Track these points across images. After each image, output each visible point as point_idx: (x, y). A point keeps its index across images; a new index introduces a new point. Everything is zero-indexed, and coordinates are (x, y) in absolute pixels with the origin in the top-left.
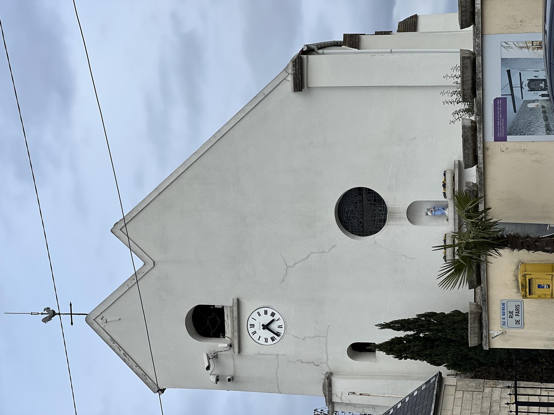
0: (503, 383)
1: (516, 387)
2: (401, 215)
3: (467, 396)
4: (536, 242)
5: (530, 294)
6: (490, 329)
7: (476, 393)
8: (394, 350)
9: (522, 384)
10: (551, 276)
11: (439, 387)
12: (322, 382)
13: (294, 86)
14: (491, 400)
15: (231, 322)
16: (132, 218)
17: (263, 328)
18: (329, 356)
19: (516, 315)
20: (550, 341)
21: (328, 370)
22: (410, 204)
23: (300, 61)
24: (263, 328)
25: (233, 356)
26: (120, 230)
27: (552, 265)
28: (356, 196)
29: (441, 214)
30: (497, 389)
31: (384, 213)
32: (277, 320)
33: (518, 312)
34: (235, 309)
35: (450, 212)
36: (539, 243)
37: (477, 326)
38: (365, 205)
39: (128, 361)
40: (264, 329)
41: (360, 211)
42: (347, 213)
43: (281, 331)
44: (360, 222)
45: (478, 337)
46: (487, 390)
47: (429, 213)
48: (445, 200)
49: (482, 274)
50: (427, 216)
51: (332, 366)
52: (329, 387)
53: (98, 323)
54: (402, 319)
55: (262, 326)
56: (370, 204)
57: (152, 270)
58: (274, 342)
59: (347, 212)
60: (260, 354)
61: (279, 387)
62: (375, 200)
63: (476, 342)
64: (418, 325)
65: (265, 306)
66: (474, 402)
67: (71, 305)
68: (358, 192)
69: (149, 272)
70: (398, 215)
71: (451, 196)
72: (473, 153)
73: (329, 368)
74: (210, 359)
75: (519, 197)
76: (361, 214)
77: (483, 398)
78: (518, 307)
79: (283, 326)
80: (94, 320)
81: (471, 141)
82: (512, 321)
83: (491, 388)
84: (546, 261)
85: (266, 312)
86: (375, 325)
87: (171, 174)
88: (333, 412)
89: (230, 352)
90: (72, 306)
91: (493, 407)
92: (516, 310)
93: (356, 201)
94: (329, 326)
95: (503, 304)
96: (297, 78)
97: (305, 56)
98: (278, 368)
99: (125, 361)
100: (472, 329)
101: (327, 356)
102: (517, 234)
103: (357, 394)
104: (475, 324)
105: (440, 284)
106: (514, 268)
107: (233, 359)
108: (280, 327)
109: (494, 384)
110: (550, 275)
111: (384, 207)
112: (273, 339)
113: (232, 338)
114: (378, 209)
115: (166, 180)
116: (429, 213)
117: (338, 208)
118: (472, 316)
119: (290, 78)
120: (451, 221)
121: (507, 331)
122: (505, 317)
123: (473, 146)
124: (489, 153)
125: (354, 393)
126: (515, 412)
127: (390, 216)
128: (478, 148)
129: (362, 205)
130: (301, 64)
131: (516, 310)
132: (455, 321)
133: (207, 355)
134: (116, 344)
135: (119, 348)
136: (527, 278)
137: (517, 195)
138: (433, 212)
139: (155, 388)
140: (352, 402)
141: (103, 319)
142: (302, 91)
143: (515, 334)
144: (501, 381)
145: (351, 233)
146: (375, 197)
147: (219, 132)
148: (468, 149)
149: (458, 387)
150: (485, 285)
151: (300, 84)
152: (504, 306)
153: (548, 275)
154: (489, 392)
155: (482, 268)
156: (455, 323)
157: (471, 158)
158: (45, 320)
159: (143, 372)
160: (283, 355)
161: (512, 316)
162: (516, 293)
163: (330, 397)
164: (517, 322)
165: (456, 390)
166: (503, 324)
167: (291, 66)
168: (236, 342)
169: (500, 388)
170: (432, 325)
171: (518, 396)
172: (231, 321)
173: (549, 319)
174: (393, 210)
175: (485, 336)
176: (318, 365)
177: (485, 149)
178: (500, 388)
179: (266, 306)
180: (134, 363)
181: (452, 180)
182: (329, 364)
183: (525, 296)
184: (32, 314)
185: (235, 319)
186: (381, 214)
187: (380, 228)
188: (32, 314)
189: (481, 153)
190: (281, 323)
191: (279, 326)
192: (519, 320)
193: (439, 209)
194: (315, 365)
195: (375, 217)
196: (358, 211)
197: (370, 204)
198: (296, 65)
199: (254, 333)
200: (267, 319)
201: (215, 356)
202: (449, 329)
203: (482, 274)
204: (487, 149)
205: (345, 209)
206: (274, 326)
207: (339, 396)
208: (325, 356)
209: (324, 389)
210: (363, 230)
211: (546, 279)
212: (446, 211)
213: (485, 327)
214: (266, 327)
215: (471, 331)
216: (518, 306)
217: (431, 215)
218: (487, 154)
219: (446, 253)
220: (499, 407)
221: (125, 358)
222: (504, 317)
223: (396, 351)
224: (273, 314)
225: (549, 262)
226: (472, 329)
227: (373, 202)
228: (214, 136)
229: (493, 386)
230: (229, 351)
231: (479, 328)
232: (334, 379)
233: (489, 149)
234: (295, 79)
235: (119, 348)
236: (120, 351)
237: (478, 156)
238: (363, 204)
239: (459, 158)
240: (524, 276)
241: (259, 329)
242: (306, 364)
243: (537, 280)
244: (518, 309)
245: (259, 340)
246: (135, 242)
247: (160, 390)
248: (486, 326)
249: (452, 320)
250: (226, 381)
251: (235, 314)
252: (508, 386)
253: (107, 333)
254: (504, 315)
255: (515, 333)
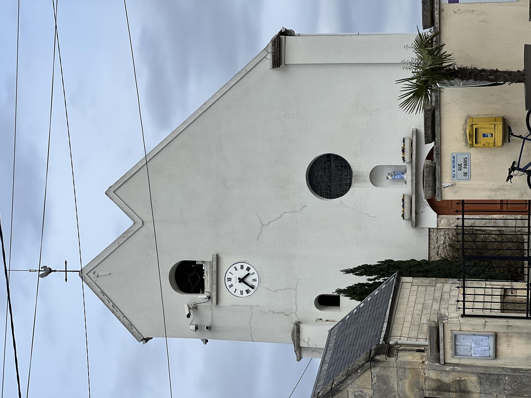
0: (452, 280)
1: (464, 287)
2: (364, 178)
3: (422, 289)
4: (482, 72)
5: (476, 143)
6: (442, 182)
7: (429, 287)
8: (357, 293)
9: (468, 283)
10: (494, 125)
11: (397, 282)
12: (291, 330)
13: (273, 63)
14: (442, 291)
15: (210, 278)
16: (125, 182)
17: (239, 281)
18: (298, 307)
19: (464, 168)
20: (493, 192)
21: (297, 320)
22: (374, 168)
23: (278, 41)
24: (239, 281)
25: (211, 307)
26: (114, 192)
27: (495, 119)
28: (325, 162)
29: (400, 178)
30: (447, 284)
31: (349, 177)
32: (252, 274)
33: (466, 164)
34: (215, 263)
35: (408, 176)
36: (484, 73)
37: (431, 179)
38: (333, 171)
39: (116, 312)
40: (240, 283)
41: (329, 176)
42: (317, 178)
43: (255, 284)
44: (329, 186)
45: (432, 190)
46: (438, 285)
47: (390, 177)
48: (404, 164)
49: (436, 128)
50: (387, 180)
51: (300, 316)
52: (297, 332)
53: (90, 278)
54: (364, 265)
55: (238, 279)
56: (337, 169)
57: (141, 229)
58: (249, 294)
59: (316, 177)
60: (236, 305)
61: (252, 336)
62: (342, 166)
63: (430, 195)
64: (379, 269)
65: (241, 262)
66: (427, 292)
67: (66, 263)
68: (327, 159)
69: (138, 231)
70: (362, 178)
71: (409, 160)
72: (431, 15)
73: (298, 317)
74: (190, 308)
75: (469, 55)
76: (329, 178)
77: (435, 290)
78: (466, 159)
79: (257, 280)
80: (87, 274)
81: (429, 4)
82: (460, 174)
83: (442, 284)
84: (490, 115)
85: (242, 267)
86: (340, 271)
87: (161, 142)
88: (301, 358)
89: (208, 304)
90: (67, 264)
91: (444, 296)
92: (464, 163)
93: (325, 167)
94: (299, 279)
95: (454, 157)
96: (276, 56)
97: (283, 37)
98: (251, 318)
99: (113, 312)
100: (427, 182)
101: (296, 306)
102: (466, 68)
103: (323, 320)
104: (429, 177)
105: (400, 104)
106: (463, 122)
107: (211, 310)
108: (254, 280)
109: (445, 281)
110: (493, 124)
111: (349, 172)
112: (248, 291)
113: (211, 292)
114: (344, 174)
115: (157, 147)
116: (390, 177)
117: (309, 173)
118: (428, 169)
119: (270, 56)
120: (409, 184)
121: (457, 183)
122: (455, 169)
123: (431, 9)
124: (443, 14)
125: (321, 319)
126: (462, 308)
127: (355, 179)
128: (435, 9)
129: (331, 171)
130: (279, 43)
131: (464, 163)
132: (411, 265)
133: (188, 305)
134: (106, 297)
135: (108, 300)
136: (473, 127)
137: (466, 53)
138: (393, 176)
139: (140, 337)
140: (318, 347)
141: (95, 274)
142: (280, 67)
143: (463, 186)
144: (451, 279)
145: (320, 196)
146: (342, 163)
147: (205, 104)
148: (426, 11)
149: (413, 283)
150: (438, 139)
151: (278, 60)
152: (454, 159)
153: (492, 124)
154: (441, 286)
155: (436, 122)
156: (411, 267)
157: (429, 19)
158: (42, 276)
159: (130, 322)
160: (257, 306)
161: (461, 168)
162: (465, 146)
163: (298, 342)
164: (465, 174)
165: (412, 285)
166: (453, 176)
167: (271, 45)
168: (214, 294)
169: (450, 283)
170: (391, 270)
171: (465, 288)
172: (210, 276)
173: (492, 170)
174: (358, 174)
175: (438, 187)
176: (288, 315)
177: (440, 11)
178: (450, 283)
179: (242, 261)
180: (122, 314)
181: (410, 145)
182: (298, 314)
183: (472, 146)
184: (30, 271)
185: (214, 273)
186: (347, 178)
187: (346, 191)
188: (30, 271)
189: (438, 14)
190: (255, 276)
191: (253, 280)
192: (467, 172)
193: (399, 173)
194: (285, 315)
195: (341, 181)
196: (327, 176)
197: (337, 169)
198: (275, 44)
199: (231, 286)
200: (242, 273)
201: (195, 308)
202: (406, 272)
203: (436, 128)
204: (443, 10)
205: (315, 174)
206: (249, 280)
207: (306, 341)
208: (294, 307)
209: (293, 335)
210: (331, 193)
211: (490, 128)
212: (404, 176)
213: (438, 179)
214: (242, 280)
215: (426, 184)
216: (466, 158)
217: (391, 178)
218: (442, 15)
219: (404, 211)
220: (449, 296)
221: (114, 309)
222: (454, 169)
223: (359, 294)
224: (248, 269)
225: (493, 116)
226: (427, 182)
227: (340, 168)
228: (201, 108)
229: (444, 282)
230: (208, 302)
231: (433, 182)
232: (303, 326)
233: (444, 10)
234: (274, 57)
235: (109, 300)
236: (109, 303)
237: (435, 16)
238: (331, 169)
239: (416, 127)
240: (472, 126)
241: (236, 282)
242: (277, 314)
243: (482, 130)
244: (466, 161)
245: (235, 293)
246: (126, 203)
247: (144, 339)
248: (439, 178)
249: (409, 265)
250: (204, 330)
251: (215, 268)
252: (456, 210)
253: (98, 286)
254: (454, 167)
255: (463, 185)
